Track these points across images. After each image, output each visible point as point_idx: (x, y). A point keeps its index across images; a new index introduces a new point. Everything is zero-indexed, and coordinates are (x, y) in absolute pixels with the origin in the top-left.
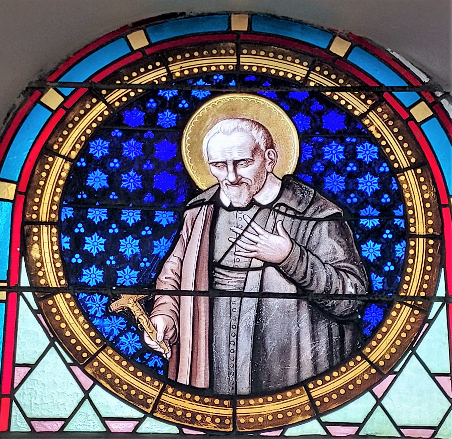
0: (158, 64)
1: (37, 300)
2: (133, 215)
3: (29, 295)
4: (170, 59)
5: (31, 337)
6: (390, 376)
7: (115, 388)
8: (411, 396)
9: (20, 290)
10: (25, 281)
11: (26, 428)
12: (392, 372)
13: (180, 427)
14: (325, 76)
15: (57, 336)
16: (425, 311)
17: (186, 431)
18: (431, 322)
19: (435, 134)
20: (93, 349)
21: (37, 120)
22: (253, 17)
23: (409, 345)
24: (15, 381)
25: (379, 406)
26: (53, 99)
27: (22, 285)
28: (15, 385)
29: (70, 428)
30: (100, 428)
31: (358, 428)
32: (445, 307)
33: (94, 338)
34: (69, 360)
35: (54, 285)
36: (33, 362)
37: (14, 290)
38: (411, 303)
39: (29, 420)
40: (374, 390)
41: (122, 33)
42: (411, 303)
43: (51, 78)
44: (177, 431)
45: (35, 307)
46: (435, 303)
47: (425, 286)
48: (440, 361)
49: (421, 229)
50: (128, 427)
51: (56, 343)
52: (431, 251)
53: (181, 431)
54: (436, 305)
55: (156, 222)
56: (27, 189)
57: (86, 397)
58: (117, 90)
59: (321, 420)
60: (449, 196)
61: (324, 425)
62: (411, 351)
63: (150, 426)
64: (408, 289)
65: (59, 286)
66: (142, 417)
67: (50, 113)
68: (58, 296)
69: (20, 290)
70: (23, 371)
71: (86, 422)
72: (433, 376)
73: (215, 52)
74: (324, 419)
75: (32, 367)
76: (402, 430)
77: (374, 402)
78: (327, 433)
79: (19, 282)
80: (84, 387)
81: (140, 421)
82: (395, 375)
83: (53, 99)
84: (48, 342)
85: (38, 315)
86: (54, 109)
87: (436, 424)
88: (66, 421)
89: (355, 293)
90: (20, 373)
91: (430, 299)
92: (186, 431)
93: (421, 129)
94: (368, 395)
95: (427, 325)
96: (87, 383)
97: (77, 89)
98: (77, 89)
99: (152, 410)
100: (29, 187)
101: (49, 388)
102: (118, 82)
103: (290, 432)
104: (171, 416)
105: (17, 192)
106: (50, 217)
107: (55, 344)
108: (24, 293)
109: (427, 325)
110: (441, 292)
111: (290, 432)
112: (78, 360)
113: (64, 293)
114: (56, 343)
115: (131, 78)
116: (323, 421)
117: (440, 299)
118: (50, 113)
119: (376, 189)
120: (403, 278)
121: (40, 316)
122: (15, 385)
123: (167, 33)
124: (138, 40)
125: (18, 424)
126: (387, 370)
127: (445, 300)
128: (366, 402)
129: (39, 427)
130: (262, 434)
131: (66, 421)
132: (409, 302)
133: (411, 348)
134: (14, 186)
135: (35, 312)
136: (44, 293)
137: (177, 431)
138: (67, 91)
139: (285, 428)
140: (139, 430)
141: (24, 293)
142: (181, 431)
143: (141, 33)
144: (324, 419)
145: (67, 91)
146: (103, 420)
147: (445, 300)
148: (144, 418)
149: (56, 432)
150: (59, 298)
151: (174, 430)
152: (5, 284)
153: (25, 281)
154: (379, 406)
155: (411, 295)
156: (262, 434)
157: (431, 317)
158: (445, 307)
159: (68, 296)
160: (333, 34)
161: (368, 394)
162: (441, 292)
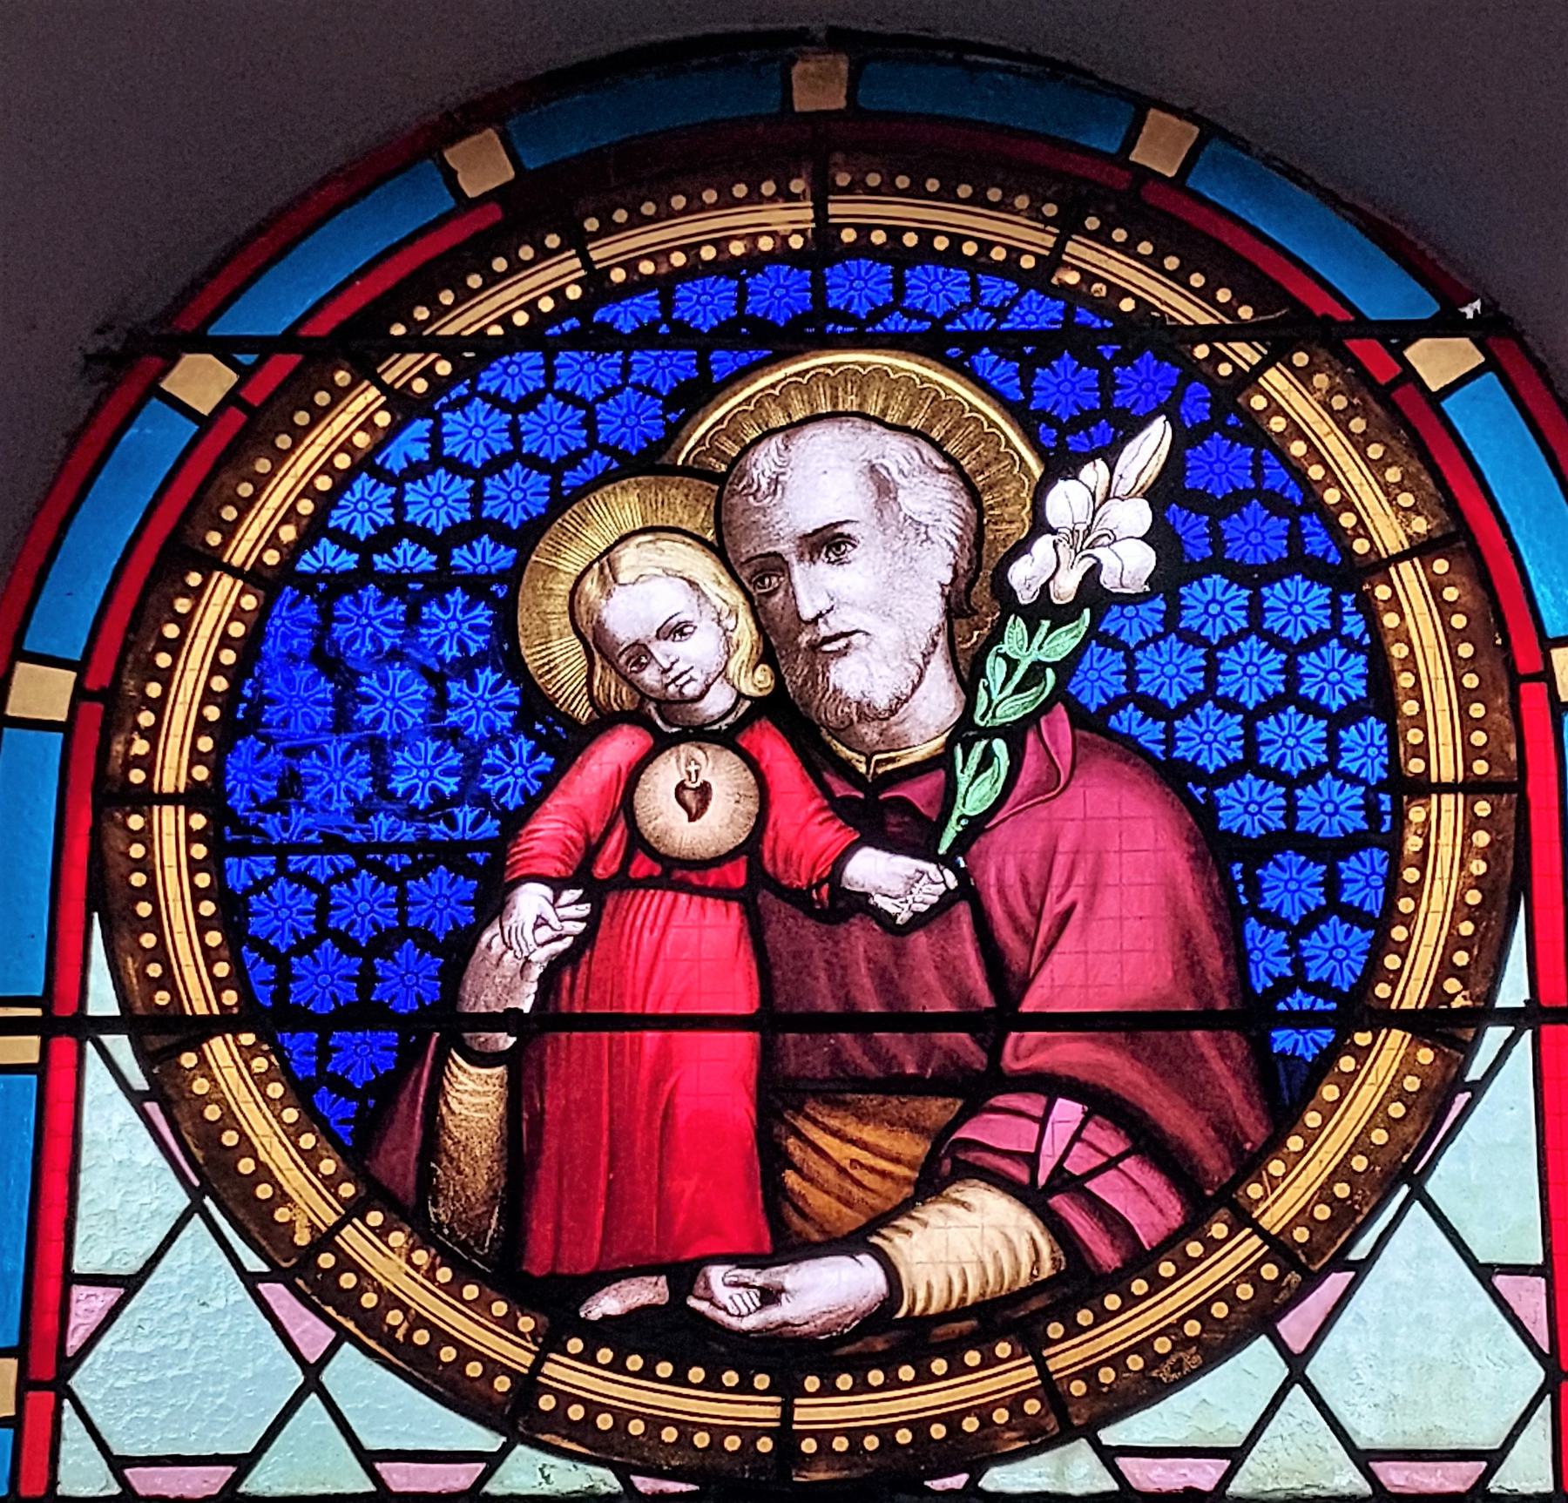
0: (553, 241)
3: (120, 1046)
4: (592, 225)
5: (125, 1181)
6: (1334, 1275)
7: (425, 1367)
8: (1418, 1341)
10: (102, 1000)
11: (101, 1482)
12: (1339, 1263)
13: (622, 1473)
15: (215, 1177)
19: (1494, 435)
20: (766, 1412)
21: (155, 443)
23: (1400, 1168)
24: (74, 1321)
25: (1298, 1387)
26: (201, 382)
27: (92, 1011)
29: (254, 1484)
30: (1349, 1480)
33: (243, 1148)
34: (254, 1263)
35: (201, 1010)
36: (133, 1265)
39: (118, 1464)
40: (1281, 1326)
41: (424, 145)
45: (139, 1082)
48: (1510, 1222)
50: (460, 1477)
51: (208, 1201)
54: (1495, 1036)
56: (112, 695)
57: (310, 1385)
58: (397, 356)
59: (1099, 1441)
61: (1108, 1456)
64: (1401, 969)
68: (217, 1042)
70: (106, 1297)
72: (1484, 1273)
74: (1111, 1436)
75: (130, 1284)
77: (1279, 1371)
80: (304, 1351)
81: (493, 1461)
82: (1351, 1274)
84: (182, 1201)
86: (205, 410)
87: (1490, 1439)
88: (244, 1463)
90: (88, 1305)
94: (1262, 1345)
96: (313, 1334)
99: (519, 1414)
101: (184, 1346)
102: (398, 330)
103: (997, 1479)
104: (592, 1443)
105: (80, 694)
106: (189, 775)
107: (205, 1209)
108: (106, 1039)
109: (1462, 1099)
110: (1513, 990)
111: (997, 1479)
112: (298, 1269)
114: (208, 1201)
115: (439, 311)
121: (152, 1107)
123: (573, 136)
124: (483, 168)
126: (1324, 1254)
128: (1259, 1363)
135: (136, 1099)
136: (164, 1034)
139: (977, 1472)
144: (1111, 1436)
146: (368, 1459)
148: (505, 1450)
150: (219, 1049)
151: (606, 1481)
152: (37, 1012)
153: (102, 1000)
154: (1298, 1387)
157: (1475, 1072)
159: (248, 1039)
161: (1263, 1344)
162: (1513, 990)
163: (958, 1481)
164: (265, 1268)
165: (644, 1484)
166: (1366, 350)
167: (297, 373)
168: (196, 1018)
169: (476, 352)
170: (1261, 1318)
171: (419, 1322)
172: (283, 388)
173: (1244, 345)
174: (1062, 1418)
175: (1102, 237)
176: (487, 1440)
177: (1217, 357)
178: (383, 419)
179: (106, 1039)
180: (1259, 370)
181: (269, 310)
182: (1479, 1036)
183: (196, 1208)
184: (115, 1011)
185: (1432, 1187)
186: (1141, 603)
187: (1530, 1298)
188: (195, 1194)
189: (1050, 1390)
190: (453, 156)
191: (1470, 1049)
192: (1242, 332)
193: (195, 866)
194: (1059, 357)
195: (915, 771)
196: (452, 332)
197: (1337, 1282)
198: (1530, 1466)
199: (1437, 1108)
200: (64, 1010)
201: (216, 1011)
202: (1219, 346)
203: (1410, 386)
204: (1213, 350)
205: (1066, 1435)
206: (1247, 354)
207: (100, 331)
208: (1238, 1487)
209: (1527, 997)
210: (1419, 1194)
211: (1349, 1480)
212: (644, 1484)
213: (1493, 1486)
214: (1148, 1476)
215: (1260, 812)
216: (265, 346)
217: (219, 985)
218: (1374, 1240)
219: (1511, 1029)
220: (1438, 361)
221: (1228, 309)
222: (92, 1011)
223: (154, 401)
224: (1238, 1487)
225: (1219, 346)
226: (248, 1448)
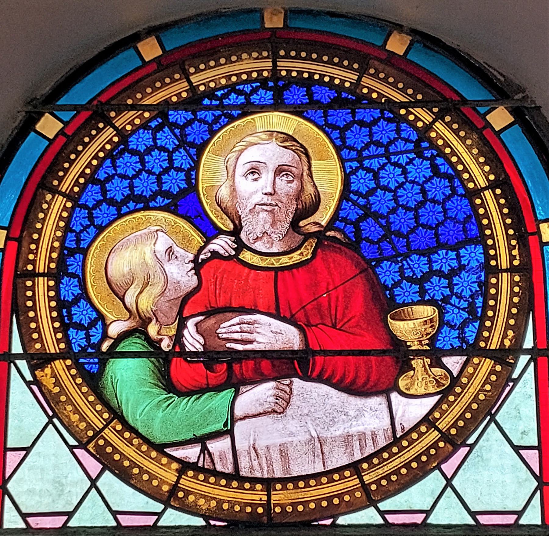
1: (32, 369)
2: (419, 267)
3: (23, 364)
5: (25, 412)
13: (206, 518)
14: (380, 79)
17: (212, 522)
18: (516, 381)
22: (291, 13)
27: (13, 352)
28: (7, 475)
34: (72, 442)
35: (53, 351)
39: (24, 516)
41: (132, 41)
43: (49, 102)
44: (204, 523)
45: (29, 378)
46: (522, 356)
50: (150, 521)
51: (55, 420)
54: (524, 359)
61: (382, 513)
62: (489, 417)
63: (173, 518)
65: (58, 351)
67: (47, 143)
68: (58, 361)
71: (93, 515)
72: (517, 449)
73: (336, 60)
75: (28, 450)
76: (118, 516)
79: (10, 349)
81: (159, 515)
83: (49, 126)
87: (427, 507)
88: (70, 515)
89: (302, 347)
90: (12, 459)
91: (517, 349)
92: (212, 522)
93: (500, 139)
95: (511, 384)
96: (94, 467)
97: (78, 112)
98: (78, 112)
103: (342, 520)
108: (17, 362)
110: (528, 343)
111: (342, 520)
113: (64, 359)
114: (55, 420)
117: (527, 352)
118: (47, 143)
121: (34, 388)
122: (7, 475)
124: (150, 50)
128: (434, 482)
129: (484, 520)
131: (70, 515)
133: (489, 413)
135: (28, 384)
136: (39, 360)
137: (204, 523)
138: (67, 116)
139: (335, 517)
140: (159, 524)
143: (152, 41)
144: (384, 506)
145: (67, 116)
149: (60, 528)
151: (199, 522)
157: (515, 376)
160: (391, 27)
162: (528, 343)
164: (77, 444)
169: (162, 110)
172: (79, 129)
176: (158, 507)
179: (17, 362)
182: (516, 359)
183: (51, 422)
184: (21, 352)
186: (253, 269)
187: (533, 457)
188: (50, 418)
189: (365, 487)
190: (140, 46)
191: (513, 366)
195: (127, 355)
197: (463, 451)
198: (533, 517)
199: (504, 382)
201: (58, 351)
207: (29, 103)
210: (493, 419)
211: (471, 522)
215: (404, 293)
217: (59, 341)
226: (71, 510)
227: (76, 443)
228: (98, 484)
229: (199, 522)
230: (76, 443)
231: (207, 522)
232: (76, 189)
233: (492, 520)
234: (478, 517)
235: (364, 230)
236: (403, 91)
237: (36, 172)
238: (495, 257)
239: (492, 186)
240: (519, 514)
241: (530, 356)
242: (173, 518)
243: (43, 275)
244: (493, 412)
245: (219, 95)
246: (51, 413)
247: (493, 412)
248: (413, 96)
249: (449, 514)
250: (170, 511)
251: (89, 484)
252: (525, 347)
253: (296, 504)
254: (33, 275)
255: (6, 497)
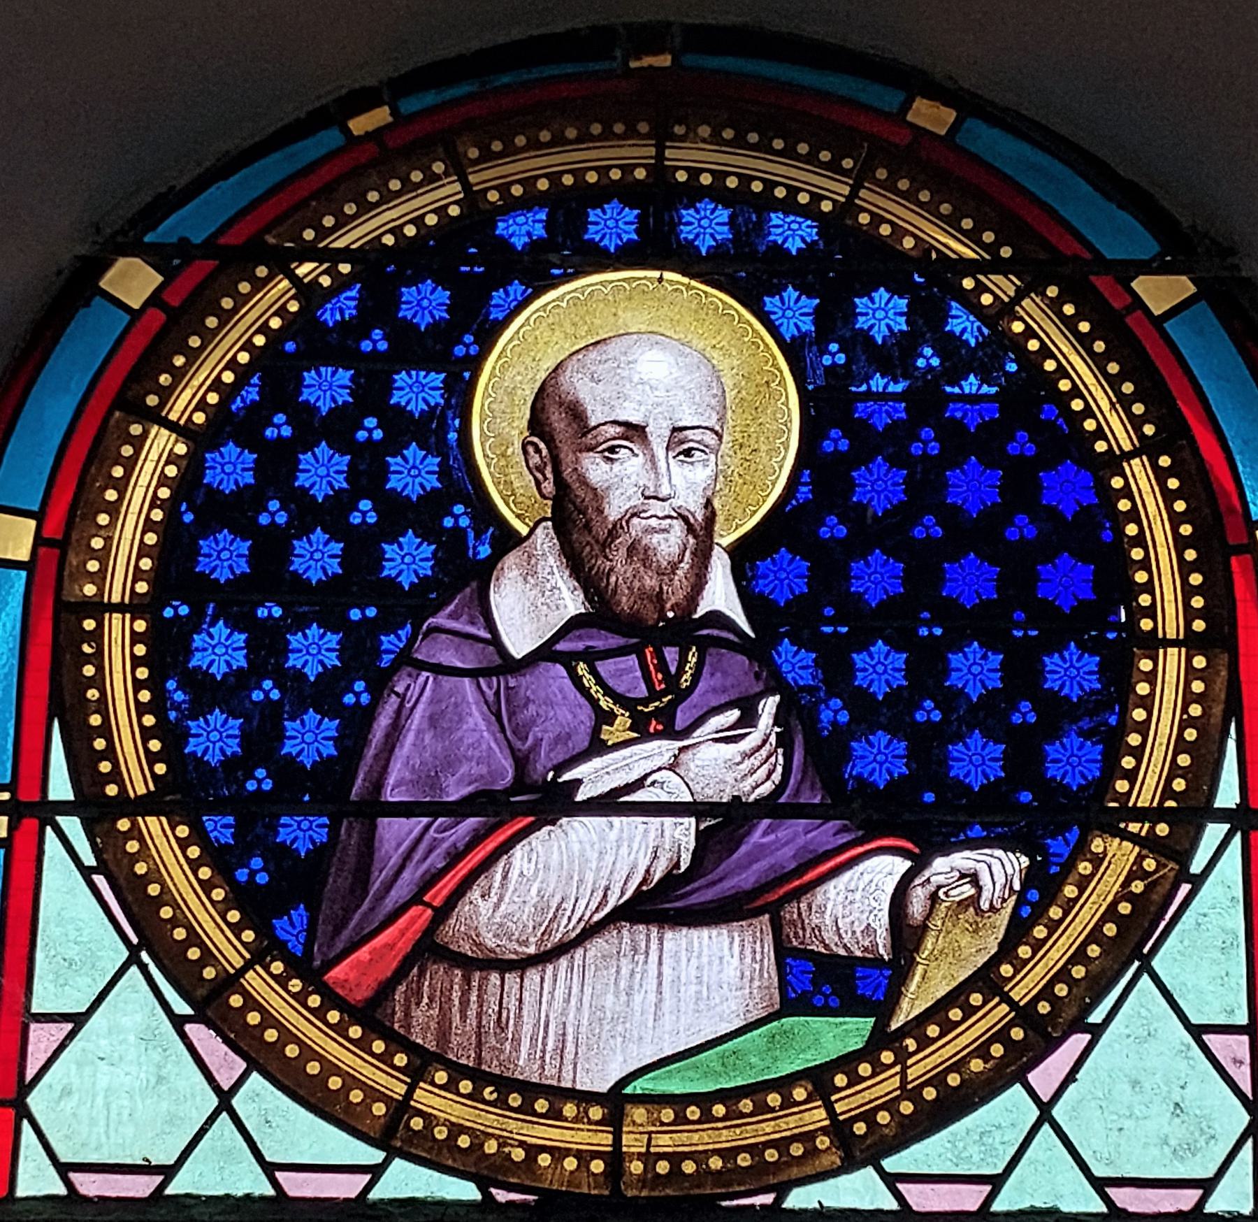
3: (72, 826)
5: (74, 928)
8: (1137, 1089)
9: (48, 812)
12: (1078, 1025)
13: (483, 1184)
16: (1177, 852)
18: (1198, 882)
19: (1209, 356)
23: (1133, 937)
27: (53, 796)
28: (30, 1074)
31: (988, 1188)
32: (1237, 839)
34: (182, 1007)
35: (151, 820)
37: (33, 812)
38: (1141, 828)
39: (64, 1170)
42: (1141, 828)
45: (89, 860)
47: (1195, 710)
48: (1221, 990)
49: (1171, 626)
50: (346, 1187)
51: (145, 956)
52: (1197, 687)
53: (487, 1196)
54: (1214, 832)
55: (338, 541)
60: (1251, 525)
61: (891, 1181)
62: (1137, 964)
63: (406, 1180)
66: (380, 1161)
67: (127, 318)
68: (141, 790)
69: (48, 812)
71: (219, 1172)
72: (1197, 1032)
75: (78, 1020)
78: (900, 1204)
81: (376, 1172)
85: (95, 877)
88: (169, 1172)
90: (42, 1039)
91: (1192, 811)
95: (1185, 888)
96: (227, 1065)
100: (70, 525)
101: (120, 1081)
105: (39, 540)
108: (59, 818)
109: (1185, 888)
110: (1228, 795)
112: (208, 1000)
114: (145, 956)
115: (323, 233)
116: (888, 1170)
117: (1223, 815)
118: (127, 318)
119: (1054, 744)
120: (1124, 713)
121: (100, 880)
122: (30, 1074)
125: (35, 1179)
127: (1239, 819)
128: (1011, 1109)
130: (724, 1204)
132: (1134, 827)
134: (32, 523)
139: (782, 1190)
141: (59, 818)
142: (487, 1196)
144: (892, 1164)
147: (1239, 819)
151: (467, 1191)
153: (60, 787)
155: (1139, 804)
156: (724, 1204)
157: (1196, 867)
158: (1237, 839)
162: (1228, 795)
163: (768, 1199)
165: (501, 1196)
166: (1102, 283)
167: (212, 277)
168: (157, 814)
170: (1013, 1067)
171: (982, 1051)
173: (1001, 277)
174: (857, 1147)
175: (889, 186)
176: (375, 1156)
177: (981, 288)
178: (1006, 970)
180: (1016, 300)
181: (192, 222)
185: (1156, 963)
188: (134, 951)
192: (998, 266)
193: (138, 685)
194: (1003, 768)
196: (342, 246)
198: (1234, 1195)
200: (28, 795)
202: (981, 277)
203: (1139, 312)
204: (978, 282)
205: (850, 1165)
206: (1006, 286)
208: (998, 1206)
209: (1238, 801)
210: (1146, 968)
212: (501, 1196)
213: (1210, 1208)
214: (922, 1198)
216: (183, 248)
218: (1106, 1012)
219: (1228, 826)
220: (1159, 292)
221: (992, 249)
222: (53, 796)
223: (98, 298)
224: (998, 1206)
225: (981, 277)
227: (188, 1011)
228: (235, 1102)
229: (467, 1191)
230: (188, 1011)
231: (483, 1188)
232: (976, 999)
233: (1137, 1198)
234: (1112, 1192)
235: (408, 402)
236: (973, 237)
237: (100, 386)
238: (248, 346)
239: (1147, 448)
240: (1207, 1186)
241: (1228, 826)
242: (406, 1180)
243: (120, 608)
244: (1145, 951)
245: (519, 242)
246: (135, 940)
247: (1145, 951)
248: (992, 249)
249: (1047, 1180)
250: (398, 1163)
251: (214, 1101)
252: (1218, 804)
253: (129, 468)
254: (99, 608)
255: (25, 1122)
